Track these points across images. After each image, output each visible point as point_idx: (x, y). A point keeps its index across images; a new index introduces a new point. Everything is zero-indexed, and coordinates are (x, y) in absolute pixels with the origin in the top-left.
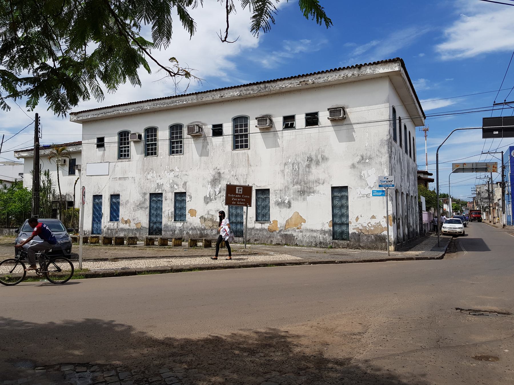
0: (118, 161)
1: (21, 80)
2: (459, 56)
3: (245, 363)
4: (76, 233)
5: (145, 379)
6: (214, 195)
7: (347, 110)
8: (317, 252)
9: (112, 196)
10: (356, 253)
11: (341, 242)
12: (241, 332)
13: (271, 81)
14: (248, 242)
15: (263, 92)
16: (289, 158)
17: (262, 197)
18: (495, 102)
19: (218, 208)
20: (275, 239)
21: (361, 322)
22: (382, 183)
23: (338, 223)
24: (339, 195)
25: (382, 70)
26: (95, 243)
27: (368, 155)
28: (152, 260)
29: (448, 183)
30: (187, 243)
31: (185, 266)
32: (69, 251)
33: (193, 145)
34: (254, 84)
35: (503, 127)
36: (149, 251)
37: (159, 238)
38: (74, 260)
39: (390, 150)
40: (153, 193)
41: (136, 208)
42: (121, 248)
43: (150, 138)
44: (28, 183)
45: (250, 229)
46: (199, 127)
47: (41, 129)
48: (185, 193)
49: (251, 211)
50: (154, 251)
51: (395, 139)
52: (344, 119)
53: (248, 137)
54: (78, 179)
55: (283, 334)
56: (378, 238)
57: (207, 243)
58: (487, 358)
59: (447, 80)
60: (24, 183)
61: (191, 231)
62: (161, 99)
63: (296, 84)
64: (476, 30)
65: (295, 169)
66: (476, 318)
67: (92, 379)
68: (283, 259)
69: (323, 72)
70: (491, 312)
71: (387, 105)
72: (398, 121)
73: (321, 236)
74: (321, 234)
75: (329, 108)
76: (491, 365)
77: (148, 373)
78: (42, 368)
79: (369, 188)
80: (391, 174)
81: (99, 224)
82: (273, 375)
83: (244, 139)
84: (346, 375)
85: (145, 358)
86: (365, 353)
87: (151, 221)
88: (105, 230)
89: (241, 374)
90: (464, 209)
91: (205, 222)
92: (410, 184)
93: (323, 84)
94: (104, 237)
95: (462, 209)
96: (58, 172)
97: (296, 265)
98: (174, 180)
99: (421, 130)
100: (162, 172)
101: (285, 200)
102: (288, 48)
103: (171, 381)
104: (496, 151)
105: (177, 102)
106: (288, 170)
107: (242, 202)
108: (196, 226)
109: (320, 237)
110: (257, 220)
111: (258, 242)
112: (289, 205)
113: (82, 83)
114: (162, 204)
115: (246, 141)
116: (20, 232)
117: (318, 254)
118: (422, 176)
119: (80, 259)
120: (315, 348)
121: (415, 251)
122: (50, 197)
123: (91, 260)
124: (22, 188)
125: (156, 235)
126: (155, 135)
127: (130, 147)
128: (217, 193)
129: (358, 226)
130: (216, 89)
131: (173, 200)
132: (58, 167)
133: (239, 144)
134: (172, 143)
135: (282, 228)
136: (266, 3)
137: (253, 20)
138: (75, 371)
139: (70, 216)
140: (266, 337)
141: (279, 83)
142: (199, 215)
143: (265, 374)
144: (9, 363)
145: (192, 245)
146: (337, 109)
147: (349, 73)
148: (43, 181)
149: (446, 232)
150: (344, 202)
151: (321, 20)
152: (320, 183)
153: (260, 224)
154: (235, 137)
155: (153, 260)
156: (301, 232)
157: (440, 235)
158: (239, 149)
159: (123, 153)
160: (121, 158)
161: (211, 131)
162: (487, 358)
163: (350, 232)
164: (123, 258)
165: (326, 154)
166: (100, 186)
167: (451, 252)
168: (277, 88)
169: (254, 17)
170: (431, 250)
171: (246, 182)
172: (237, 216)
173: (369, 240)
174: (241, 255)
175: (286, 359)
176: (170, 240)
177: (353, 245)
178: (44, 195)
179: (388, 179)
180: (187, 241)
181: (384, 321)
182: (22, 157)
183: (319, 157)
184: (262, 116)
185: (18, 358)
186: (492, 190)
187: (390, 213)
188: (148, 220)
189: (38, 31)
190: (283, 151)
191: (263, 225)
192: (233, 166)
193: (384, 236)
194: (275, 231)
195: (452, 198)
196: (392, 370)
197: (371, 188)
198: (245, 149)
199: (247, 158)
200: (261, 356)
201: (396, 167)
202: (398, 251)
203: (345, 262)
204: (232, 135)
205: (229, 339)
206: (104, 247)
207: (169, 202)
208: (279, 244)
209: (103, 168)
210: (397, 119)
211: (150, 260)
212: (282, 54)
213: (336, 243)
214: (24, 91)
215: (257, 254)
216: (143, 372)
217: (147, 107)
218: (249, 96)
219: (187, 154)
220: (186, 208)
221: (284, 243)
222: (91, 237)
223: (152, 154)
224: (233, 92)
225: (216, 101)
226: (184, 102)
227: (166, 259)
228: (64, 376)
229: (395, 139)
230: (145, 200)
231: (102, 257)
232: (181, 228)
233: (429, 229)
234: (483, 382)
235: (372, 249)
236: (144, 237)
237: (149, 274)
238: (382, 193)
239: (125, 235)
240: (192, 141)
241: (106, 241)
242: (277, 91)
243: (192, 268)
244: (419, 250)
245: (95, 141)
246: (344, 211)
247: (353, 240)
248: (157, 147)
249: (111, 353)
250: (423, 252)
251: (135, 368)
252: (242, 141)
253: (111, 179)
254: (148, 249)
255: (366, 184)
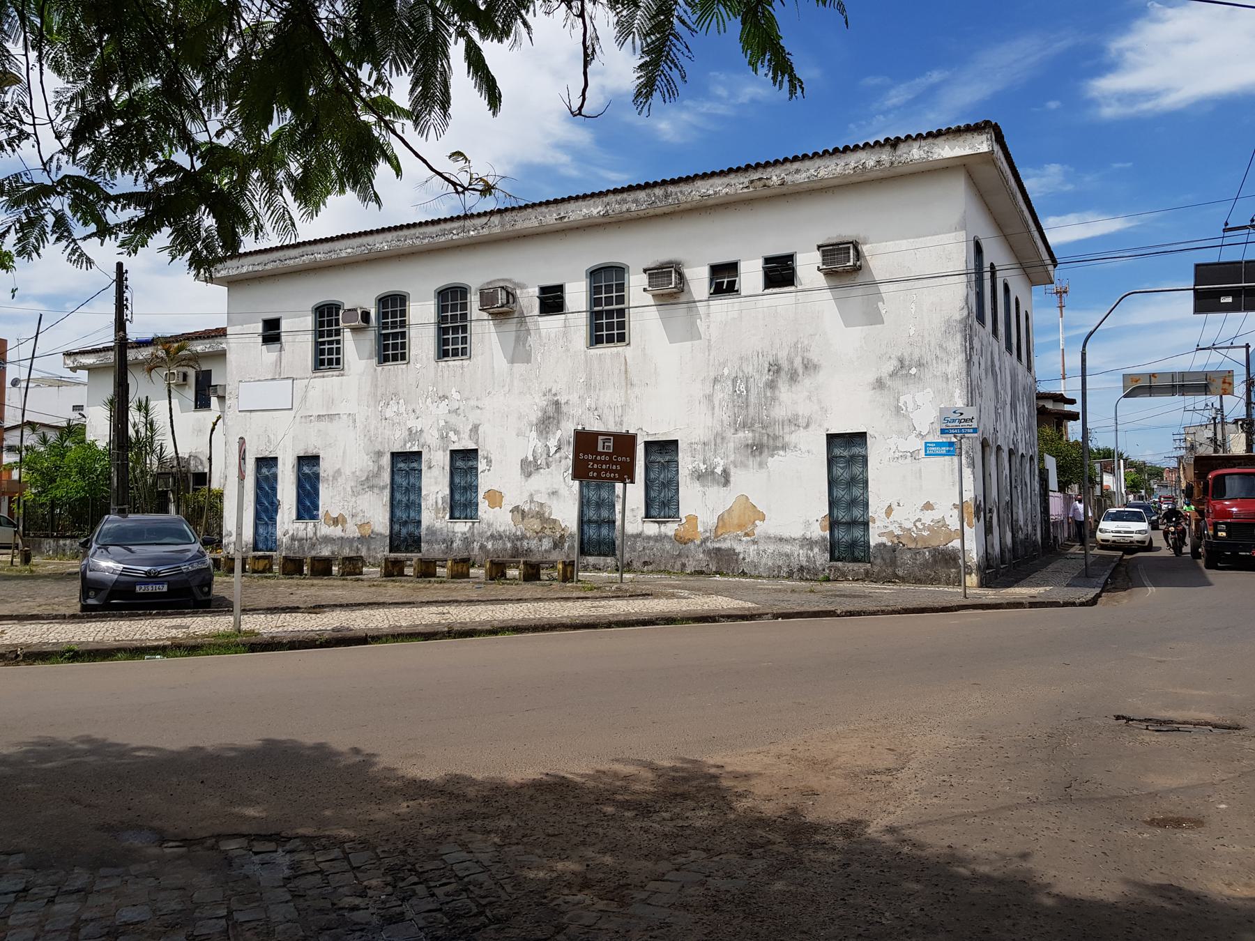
0: (314, 375)
1: (116, 198)
2: (1146, 106)
3: (628, 834)
4: (216, 550)
5: (409, 867)
6: (545, 456)
7: (865, 249)
8: (793, 591)
9: (300, 458)
10: (886, 592)
11: (851, 566)
12: (618, 767)
13: (680, 180)
14: (628, 567)
15: (662, 207)
16: (724, 365)
17: (659, 459)
18: (1226, 224)
19: (555, 486)
20: (691, 559)
21: (892, 747)
22: (949, 424)
23: (844, 520)
24: (845, 454)
25: (947, 150)
26: (263, 571)
27: (916, 357)
28: (403, 610)
29: (1114, 421)
30: (482, 571)
31: (480, 623)
32: (206, 589)
33: (494, 336)
34: (639, 187)
35: (1244, 287)
36: (394, 590)
37: (415, 559)
38: (220, 611)
39: (968, 344)
40: (400, 451)
41: (360, 488)
42: (325, 582)
43: (390, 320)
44: (99, 430)
45: (632, 536)
46: (508, 293)
47: (130, 301)
48: (476, 451)
49: (633, 495)
50: (405, 590)
51: (981, 318)
52: (857, 269)
53: (627, 315)
54: (219, 418)
55: (713, 771)
56: (940, 556)
57: (530, 571)
58: (1177, 823)
59: (1116, 166)
60: (88, 428)
61: (490, 543)
62: (414, 225)
63: (741, 186)
64: (1188, 40)
65: (738, 392)
66: (1162, 738)
67: (291, 867)
68: (712, 607)
69: (805, 157)
70: (1198, 724)
71: (962, 235)
72: (987, 276)
73: (801, 552)
74: (802, 547)
75: (820, 243)
76: (1185, 835)
77: (414, 854)
78: (177, 844)
79: (917, 436)
80: (970, 403)
81: (270, 527)
82: (691, 859)
83: (615, 320)
84: (856, 857)
85: (405, 823)
86: (899, 811)
87: (395, 520)
88: (284, 540)
89: (621, 855)
90: (1155, 486)
91: (523, 519)
92: (1019, 425)
93: (805, 186)
94: (285, 558)
95: (1150, 485)
96: (170, 404)
97: (743, 620)
98: (448, 420)
99: (1050, 291)
100: (420, 401)
101: (715, 468)
102: (721, 91)
103: (467, 869)
104: (1232, 343)
105: (454, 232)
106: (722, 394)
107: (611, 471)
108: (501, 529)
109: (801, 555)
110: (648, 515)
111: (650, 568)
112: (726, 479)
113: (249, 201)
114: (420, 477)
115: (622, 325)
116: (91, 545)
117: (796, 595)
118: (1050, 405)
119: (237, 608)
120: (785, 802)
121: (1029, 586)
122: (153, 463)
123: (261, 610)
124: (83, 441)
125: (408, 552)
126: (403, 313)
127: (342, 342)
128: (553, 450)
129: (891, 528)
130: (547, 201)
131: (447, 468)
132: (170, 391)
133: (605, 333)
134: (442, 331)
135: (708, 534)
136: (668, 36)
137: (639, 75)
138: (251, 850)
139: (202, 509)
140: (674, 779)
141: (699, 183)
142: (508, 504)
143: (674, 855)
144: (105, 832)
145: (494, 574)
146: (841, 246)
147: (869, 159)
148: (135, 425)
149: (1108, 541)
150: (857, 470)
151: (782, 78)
152: (799, 426)
153: (656, 525)
154: (595, 316)
155: (405, 610)
156: (755, 542)
157: (1092, 548)
158: (605, 345)
159: (326, 357)
160: (322, 367)
161: (537, 302)
162: (1177, 823)
163: (872, 543)
164: (336, 606)
165: (814, 356)
166: (272, 437)
167: (1116, 589)
168: (696, 196)
169: (640, 67)
170: (1068, 585)
171: (621, 424)
172: (599, 505)
173: (918, 562)
174: (613, 597)
175: (721, 824)
176: (440, 563)
177: (878, 575)
178: (138, 458)
179: (962, 414)
180: (481, 566)
181: (947, 745)
182: (83, 367)
183: (798, 362)
184: (658, 264)
185: (122, 823)
186: (1224, 440)
187: (969, 495)
188: (387, 516)
189: (156, 89)
190: (709, 348)
191: (663, 527)
192: (588, 386)
193: (954, 551)
194: (692, 541)
195: (1125, 460)
196: (958, 847)
197: (923, 437)
198: (619, 344)
199: (623, 368)
200: (664, 819)
201: (983, 385)
202: (987, 587)
203: (859, 613)
204: (586, 311)
205: (591, 784)
206: (285, 581)
207: (438, 472)
208: (701, 573)
209: (279, 393)
210: (985, 270)
211: (399, 610)
212: (707, 107)
213: (837, 569)
214: (124, 223)
215: (649, 595)
216: (404, 852)
217: (382, 244)
218: (627, 215)
219: (479, 358)
220: (477, 487)
221: (714, 569)
222: (254, 557)
223: (395, 358)
224: (588, 207)
225: (548, 228)
226: (472, 233)
227: (435, 608)
228: (228, 861)
229: (981, 318)
230: (380, 468)
231: (283, 602)
232: (468, 535)
233: (1066, 535)
234: (1162, 871)
235: (925, 583)
236: (379, 556)
237: (397, 642)
238: (948, 449)
239: (333, 553)
240: (490, 326)
241: (290, 566)
242: (694, 203)
243: (497, 628)
244: (1038, 585)
245: (259, 327)
246: (857, 492)
247: (879, 561)
248: (407, 340)
249: (328, 813)
250: (1048, 588)
251: (383, 843)
252: (610, 326)
253: (298, 418)
254: (390, 584)
255: (911, 427)
